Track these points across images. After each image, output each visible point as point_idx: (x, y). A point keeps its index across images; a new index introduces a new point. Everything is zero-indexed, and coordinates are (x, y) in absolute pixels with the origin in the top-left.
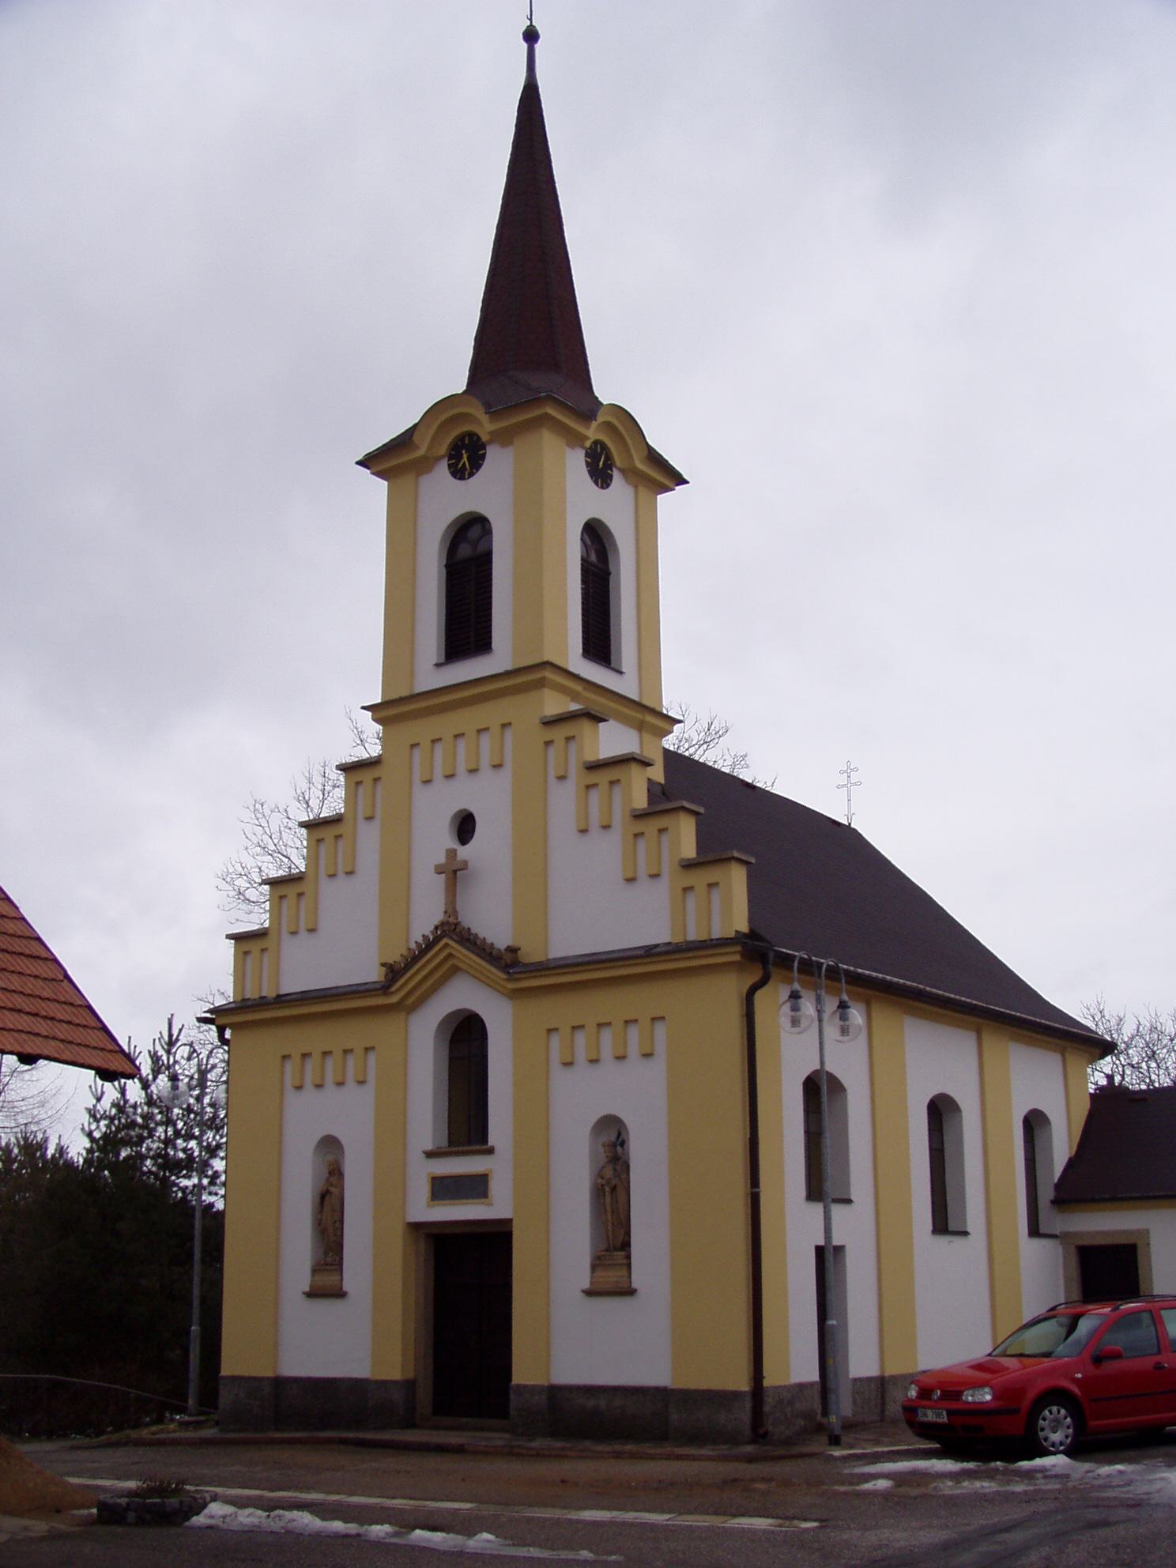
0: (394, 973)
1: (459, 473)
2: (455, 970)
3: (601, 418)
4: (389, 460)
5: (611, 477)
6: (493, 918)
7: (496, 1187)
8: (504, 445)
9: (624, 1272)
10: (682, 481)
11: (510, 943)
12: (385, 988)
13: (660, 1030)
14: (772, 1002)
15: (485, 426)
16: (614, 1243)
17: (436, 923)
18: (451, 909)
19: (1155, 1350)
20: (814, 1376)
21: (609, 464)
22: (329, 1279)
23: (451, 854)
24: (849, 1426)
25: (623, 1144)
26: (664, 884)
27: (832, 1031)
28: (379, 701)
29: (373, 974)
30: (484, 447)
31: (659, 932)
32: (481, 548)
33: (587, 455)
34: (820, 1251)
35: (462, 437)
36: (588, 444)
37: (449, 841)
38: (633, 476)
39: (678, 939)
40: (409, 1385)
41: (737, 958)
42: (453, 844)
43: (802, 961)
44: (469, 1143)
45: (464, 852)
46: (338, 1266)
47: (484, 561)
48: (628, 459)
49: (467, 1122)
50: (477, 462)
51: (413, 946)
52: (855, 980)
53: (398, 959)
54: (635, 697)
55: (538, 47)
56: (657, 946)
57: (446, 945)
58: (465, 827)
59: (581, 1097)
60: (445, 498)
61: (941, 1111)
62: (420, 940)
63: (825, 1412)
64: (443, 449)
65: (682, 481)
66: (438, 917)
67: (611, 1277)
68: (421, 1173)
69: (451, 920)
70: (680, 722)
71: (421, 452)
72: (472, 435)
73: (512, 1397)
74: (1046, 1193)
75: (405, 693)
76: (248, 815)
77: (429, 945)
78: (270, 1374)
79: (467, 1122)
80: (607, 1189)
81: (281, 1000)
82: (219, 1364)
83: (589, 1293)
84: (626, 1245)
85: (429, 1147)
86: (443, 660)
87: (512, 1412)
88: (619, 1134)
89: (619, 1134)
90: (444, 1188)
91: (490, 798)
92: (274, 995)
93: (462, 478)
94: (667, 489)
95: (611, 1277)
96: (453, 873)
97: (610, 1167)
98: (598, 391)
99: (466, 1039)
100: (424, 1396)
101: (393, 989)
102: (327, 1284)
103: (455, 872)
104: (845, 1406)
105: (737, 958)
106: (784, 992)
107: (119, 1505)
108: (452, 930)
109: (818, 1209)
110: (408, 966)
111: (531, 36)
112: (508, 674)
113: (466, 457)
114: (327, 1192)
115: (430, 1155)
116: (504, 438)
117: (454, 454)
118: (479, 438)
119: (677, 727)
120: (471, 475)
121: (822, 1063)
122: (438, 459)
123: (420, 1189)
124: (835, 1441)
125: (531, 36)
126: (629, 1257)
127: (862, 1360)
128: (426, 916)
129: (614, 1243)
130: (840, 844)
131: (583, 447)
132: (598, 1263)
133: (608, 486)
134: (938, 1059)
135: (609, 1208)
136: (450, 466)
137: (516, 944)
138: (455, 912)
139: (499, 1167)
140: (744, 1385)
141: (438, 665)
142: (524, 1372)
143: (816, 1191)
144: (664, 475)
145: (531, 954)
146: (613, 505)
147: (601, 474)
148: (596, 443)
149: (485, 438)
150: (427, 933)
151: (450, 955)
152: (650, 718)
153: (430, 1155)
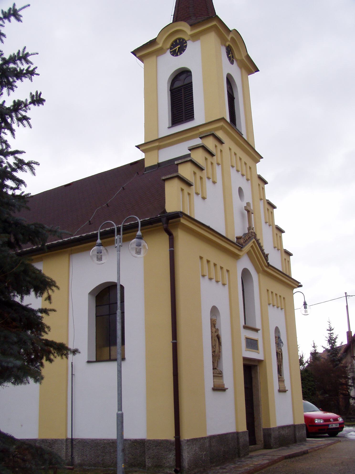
4: (144, 52)
8: (194, 41)
19: (248, 325)
28: (143, 142)
32: (186, 82)
43: (101, 233)
47: (189, 87)
48: (233, 46)
50: (182, 49)
60: (169, 64)
64: (169, 45)
65: (257, 70)
71: (160, 46)
75: (157, 138)
93: (177, 55)
107: (349, 426)
113: (178, 47)
116: (195, 37)
117: (174, 44)
136: (171, 52)
141: (169, 128)
147: (231, 59)
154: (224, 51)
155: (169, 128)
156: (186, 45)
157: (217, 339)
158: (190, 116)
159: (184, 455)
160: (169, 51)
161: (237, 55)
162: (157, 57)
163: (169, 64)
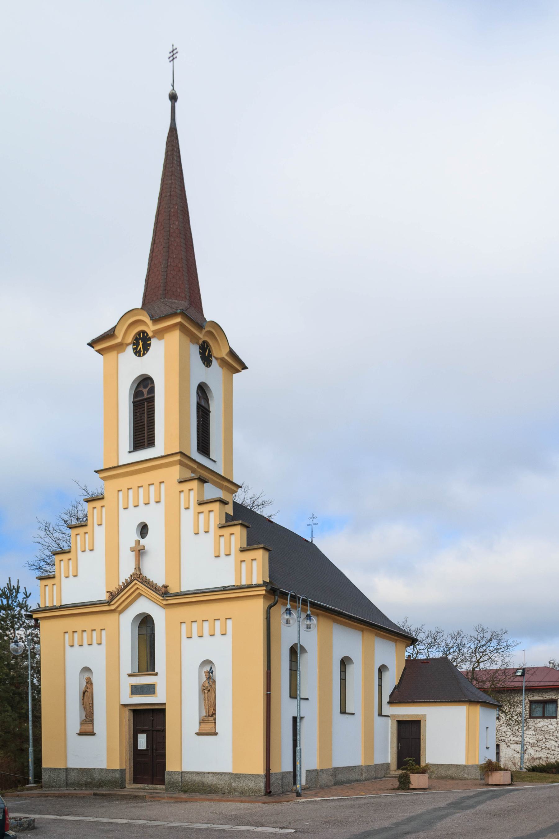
0: (112, 596)
1: (138, 353)
2: (140, 595)
3: (207, 329)
4: (104, 343)
5: (211, 361)
6: (156, 572)
7: (158, 689)
9: (213, 725)
10: (245, 368)
11: (164, 584)
12: (108, 603)
13: (229, 622)
14: (279, 612)
15: (150, 328)
16: (209, 716)
17: (131, 574)
18: (138, 568)
20: (291, 769)
21: (210, 355)
22: (87, 728)
23: (138, 542)
24: (303, 789)
25: (212, 672)
26: (232, 558)
27: (303, 628)
29: (104, 597)
30: (150, 339)
31: (230, 582)
33: (200, 348)
34: (295, 719)
35: (139, 333)
36: (201, 342)
37: (137, 537)
38: (223, 363)
39: (238, 584)
40: (122, 771)
41: (264, 592)
42: (138, 538)
44: (147, 671)
45: (143, 542)
46: (92, 722)
48: (208, 343)
49: (146, 660)
50: (146, 347)
51: (121, 584)
52: (313, 605)
53: (115, 590)
54: (223, 475)
55: (177, 104)
56: (228, 586)
57: (136, 584)
58: (144, 530)
59: (194, 652)
60: (130, 366)
61: (345, 662)
62: (124, 581)
63: (295, 783)
65: (245, 368)
66: (132, 570)
67: (208, 727)
68: (126, 683)
69: (138, 572)
70: (241, 487)
71: (119, 340)
72: (144, 332)
73: (166, 776)
74: (386, 698)
75: (116, 465)
76: (43, 534)
77: (127, 584)
78: (63, 766)
79: (146, 660)
80: (206, 691)
81: (62, 607)
82: (41, 764)
83: (198, 734)
84: (214, 714)
85: (130, 672)
86: (132, 450)
87: (166, 782)
88: (211, 668)
89: (211, 668)
90: (136, 690)
91: (155, 517)
92: (59, 605)
93: (140, 356)
94: (238, 371)
95: (208, 727)
96: (140, 552)
97: (207, 681)
98: (205, 316)
99: (145, 623)
100: (129, 776)
101: (112, 603)
102: (87, 730)
103: (139, 550)
104: (303, 780)
105: (264, 592)
106: (283, 609)
108: (138, 577)
109: (295, 701)
110: (118, 594)
111: (173, 98)
112: (162, 457)
113: (142, 344)
114: (86, 691)
115: (130, 675)
116: (160, 334)
117: (135, 343)
118: (147, 335)
119: (239, 490)
120: (144, 354)
121: (299, 640)
122: (128, 345)
123: (126, 690)
124: (299, 795)
125: (173, 98)
126: (215, 719)
127: (310, 761)
128: (127, 570)
129: (209, 716)
130: (308, 548)
131: (197, 343)
132: (202, 721)
133: (210, 366)
134: (347, 642)
135: (207, 699)
136: (134, 349)
137: (167, 584)
138: (139, 569)
139: (159, 680)
140: (261, 770)
141: (130, 452)
142: (171, 766)
143: (293, 695)
144: (235, 364)
145: (173, 589)
146: (213, 376)
147: (207, 360)
148: (204, 342)
149: (150, 334)
150: (127, 578)
151: (138, 588)
152: (226, 484)
153: (130, 675)
154: (195, 351)
155: (130, 452)
156: (150, 343)
157: (87, 695)
158: (151, 443)
159: (210, 783)
160: (130, 348)
161: (216, 352)
162: (118, 353)
163: (130, 366)
